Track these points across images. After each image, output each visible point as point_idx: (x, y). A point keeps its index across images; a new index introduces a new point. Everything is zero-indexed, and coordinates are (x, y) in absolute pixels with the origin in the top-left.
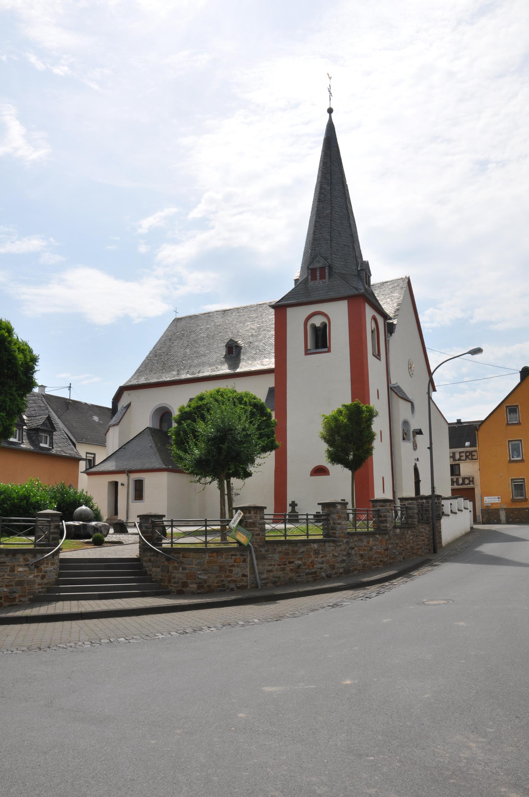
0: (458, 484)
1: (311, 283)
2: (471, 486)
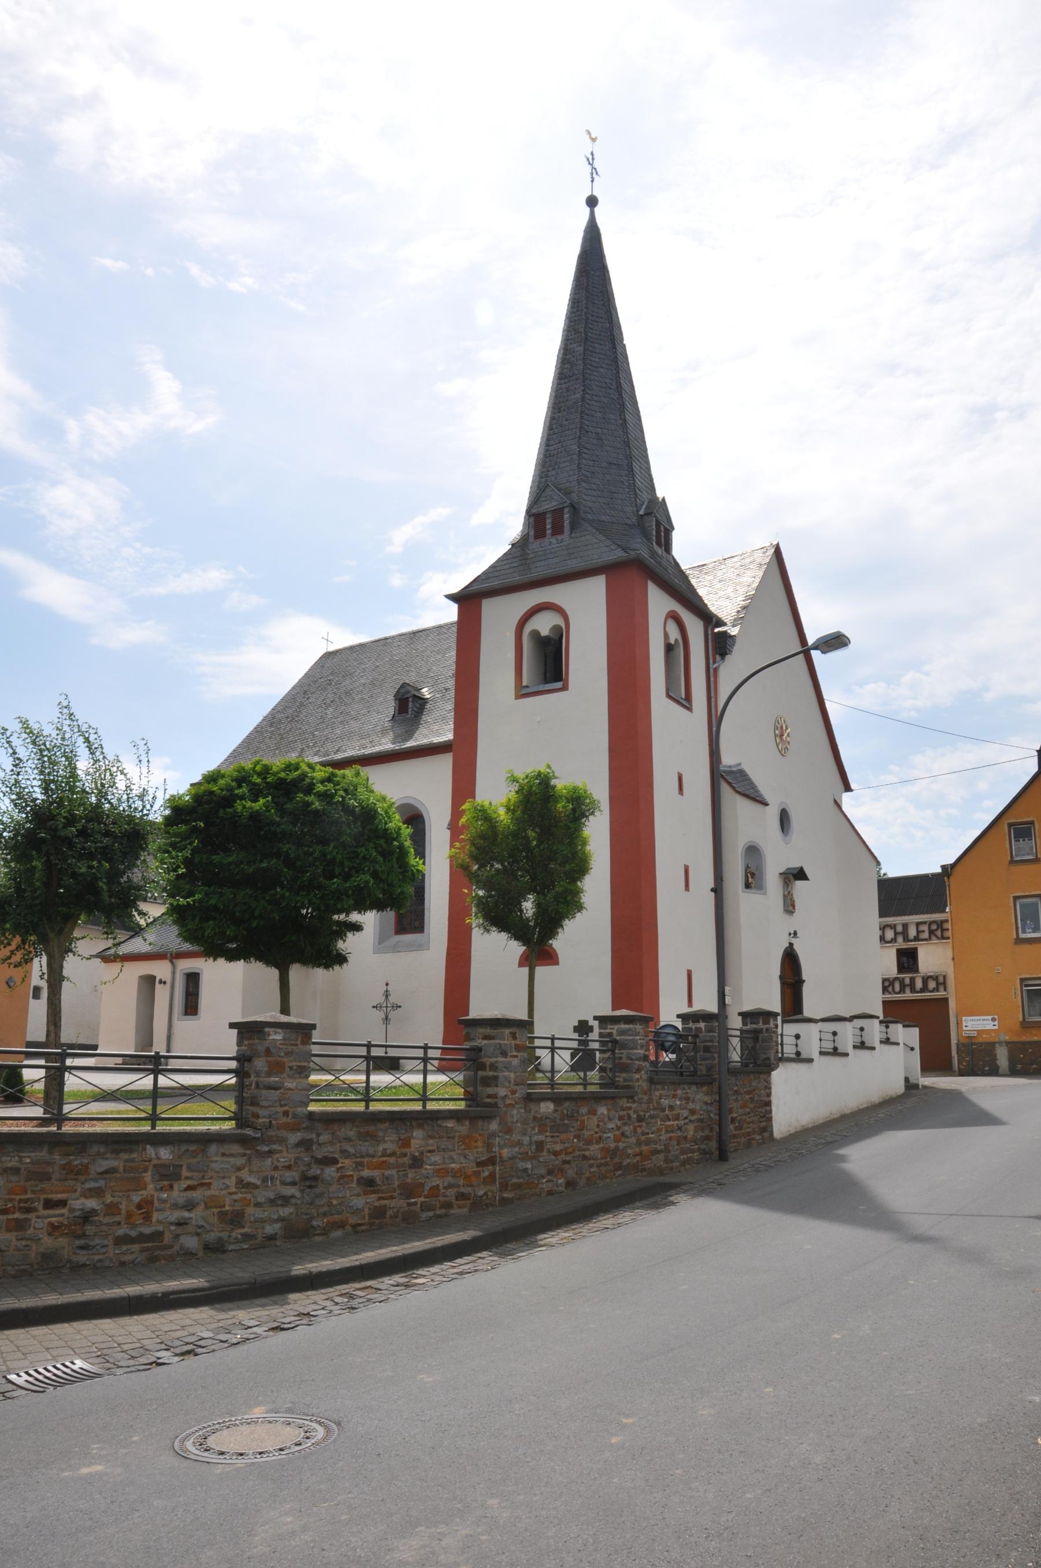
0: (913, 990)
1: (535, 545)
2: (941, 994)
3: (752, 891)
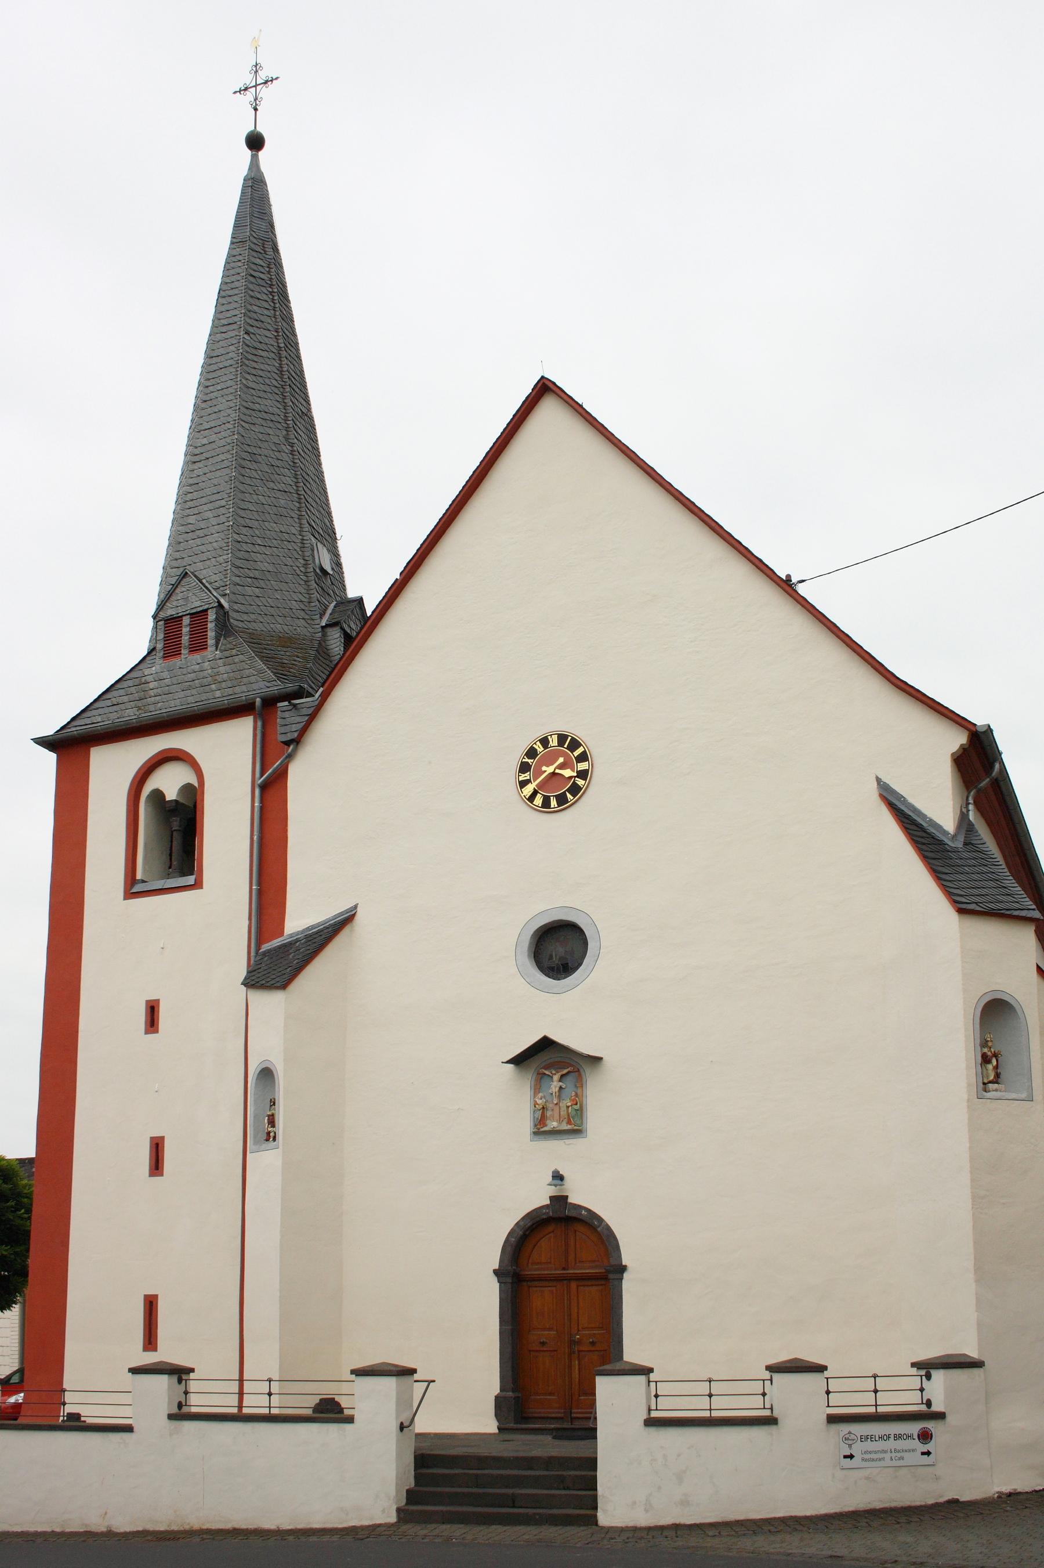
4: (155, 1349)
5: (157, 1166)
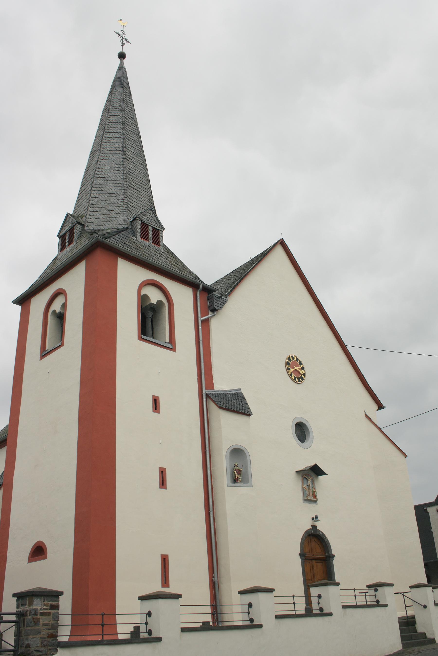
3: (238, 484)
4: (168, 586)
5: (163, 483)
